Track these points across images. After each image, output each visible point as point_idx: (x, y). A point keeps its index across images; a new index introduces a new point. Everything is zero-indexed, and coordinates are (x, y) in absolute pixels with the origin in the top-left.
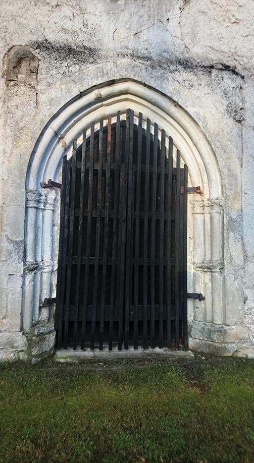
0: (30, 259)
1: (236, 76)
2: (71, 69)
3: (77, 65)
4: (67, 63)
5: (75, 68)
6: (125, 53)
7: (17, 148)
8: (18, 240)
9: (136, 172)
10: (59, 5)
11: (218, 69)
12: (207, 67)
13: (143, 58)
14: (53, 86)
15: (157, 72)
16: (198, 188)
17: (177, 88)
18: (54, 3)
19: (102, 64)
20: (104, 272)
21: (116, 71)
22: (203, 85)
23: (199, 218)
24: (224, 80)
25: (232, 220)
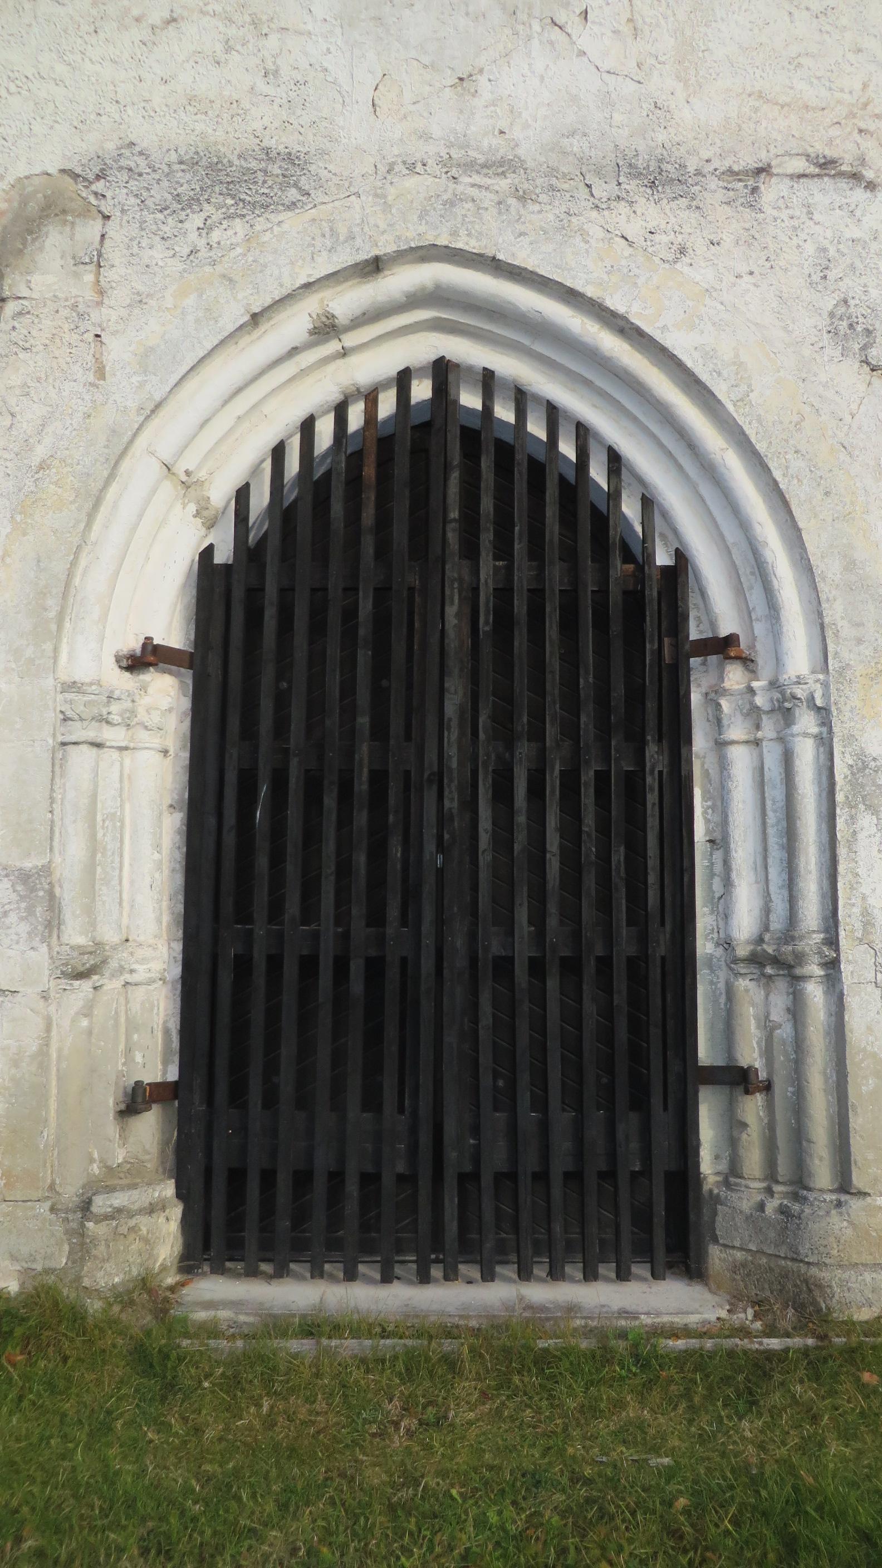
0: (75, 935)
1: (868, 194)
2: (216, 235)
3: (238, 220)
4: (203, 215)
5: (230, 232)
6: (418, 156)
7: (25, 534)
8: (28, 864)
9: (476, 590)
10: (174, 20)
11: (791, 177)
12: (746, 173)
13: (484, 166)
14: (152, 302)
15: (540, 212)
16: (731, 640)
17: (624, 262)
18: (156, 17)
19: (329, 206)
20: (357, 986)
21: (383, 226)
22: (728, 240)
23: (741, 759)
24: (817, 217)
25: (865, 767)
